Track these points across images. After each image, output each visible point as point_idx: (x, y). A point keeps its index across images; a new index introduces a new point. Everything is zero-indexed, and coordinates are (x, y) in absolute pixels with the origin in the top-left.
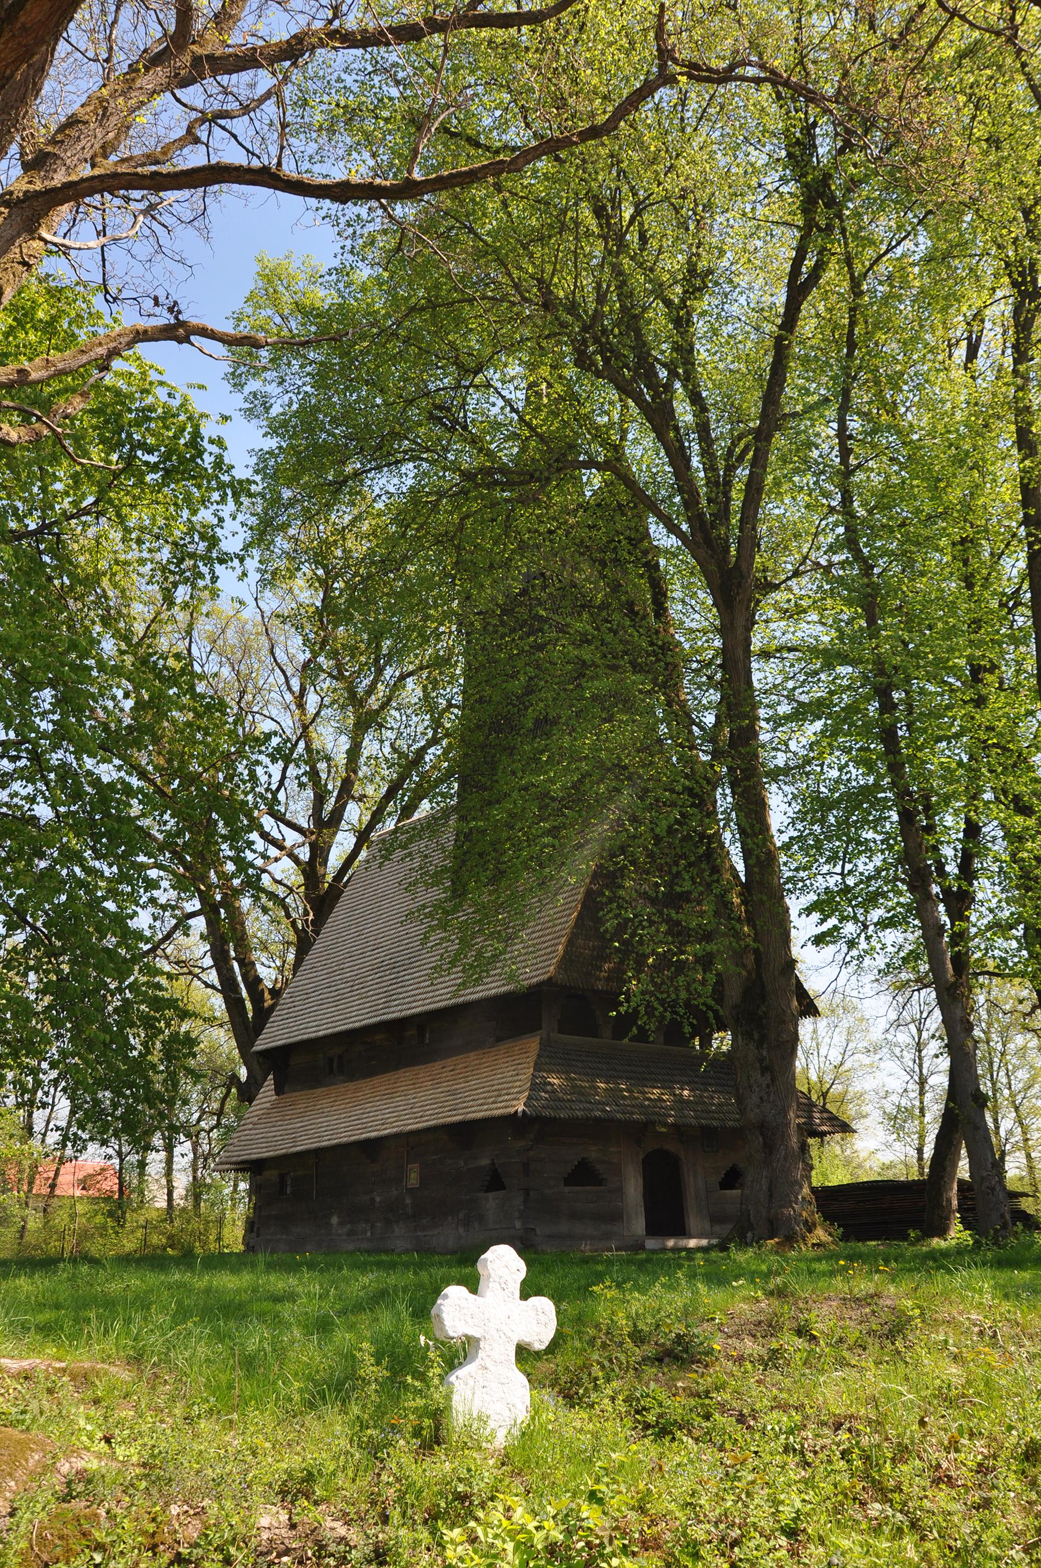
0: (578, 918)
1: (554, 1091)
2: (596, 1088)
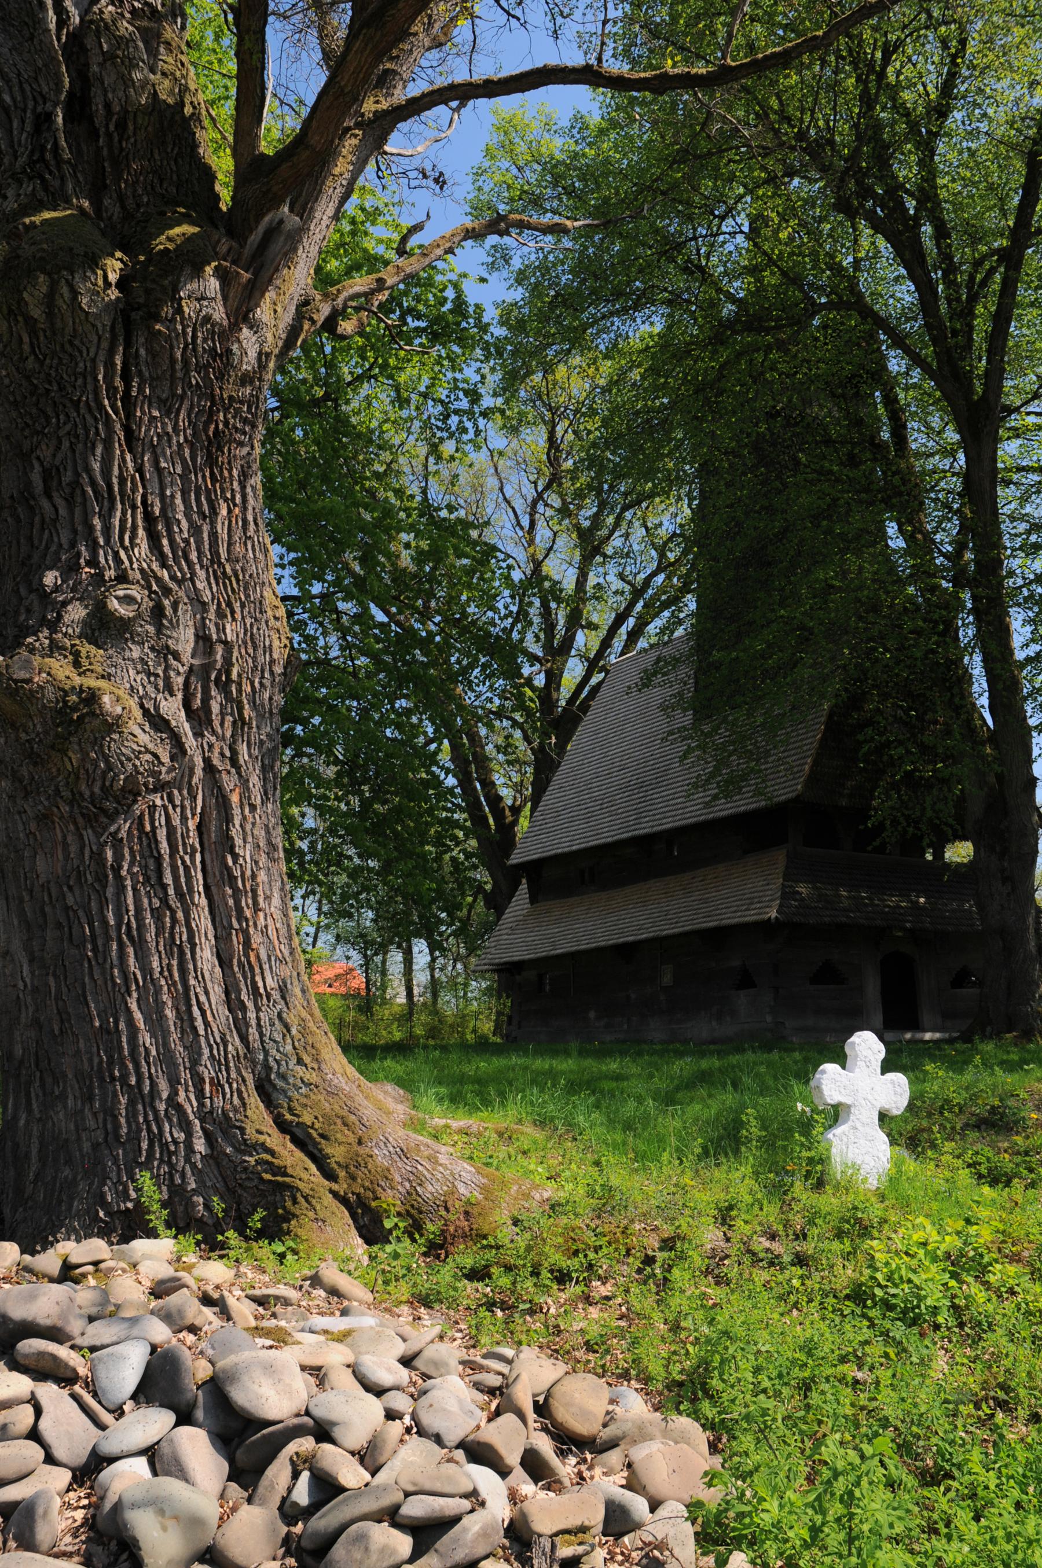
0: (822, 740)
1: (803, 899)
2: (840, 896)
